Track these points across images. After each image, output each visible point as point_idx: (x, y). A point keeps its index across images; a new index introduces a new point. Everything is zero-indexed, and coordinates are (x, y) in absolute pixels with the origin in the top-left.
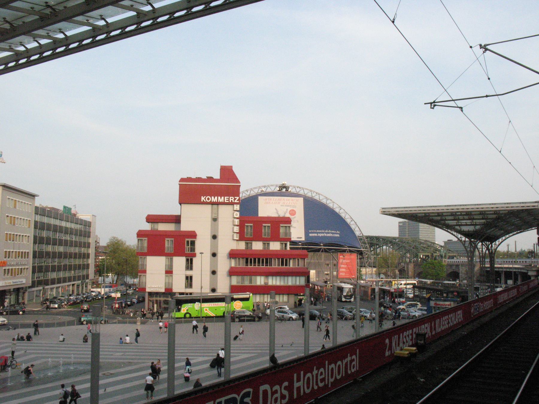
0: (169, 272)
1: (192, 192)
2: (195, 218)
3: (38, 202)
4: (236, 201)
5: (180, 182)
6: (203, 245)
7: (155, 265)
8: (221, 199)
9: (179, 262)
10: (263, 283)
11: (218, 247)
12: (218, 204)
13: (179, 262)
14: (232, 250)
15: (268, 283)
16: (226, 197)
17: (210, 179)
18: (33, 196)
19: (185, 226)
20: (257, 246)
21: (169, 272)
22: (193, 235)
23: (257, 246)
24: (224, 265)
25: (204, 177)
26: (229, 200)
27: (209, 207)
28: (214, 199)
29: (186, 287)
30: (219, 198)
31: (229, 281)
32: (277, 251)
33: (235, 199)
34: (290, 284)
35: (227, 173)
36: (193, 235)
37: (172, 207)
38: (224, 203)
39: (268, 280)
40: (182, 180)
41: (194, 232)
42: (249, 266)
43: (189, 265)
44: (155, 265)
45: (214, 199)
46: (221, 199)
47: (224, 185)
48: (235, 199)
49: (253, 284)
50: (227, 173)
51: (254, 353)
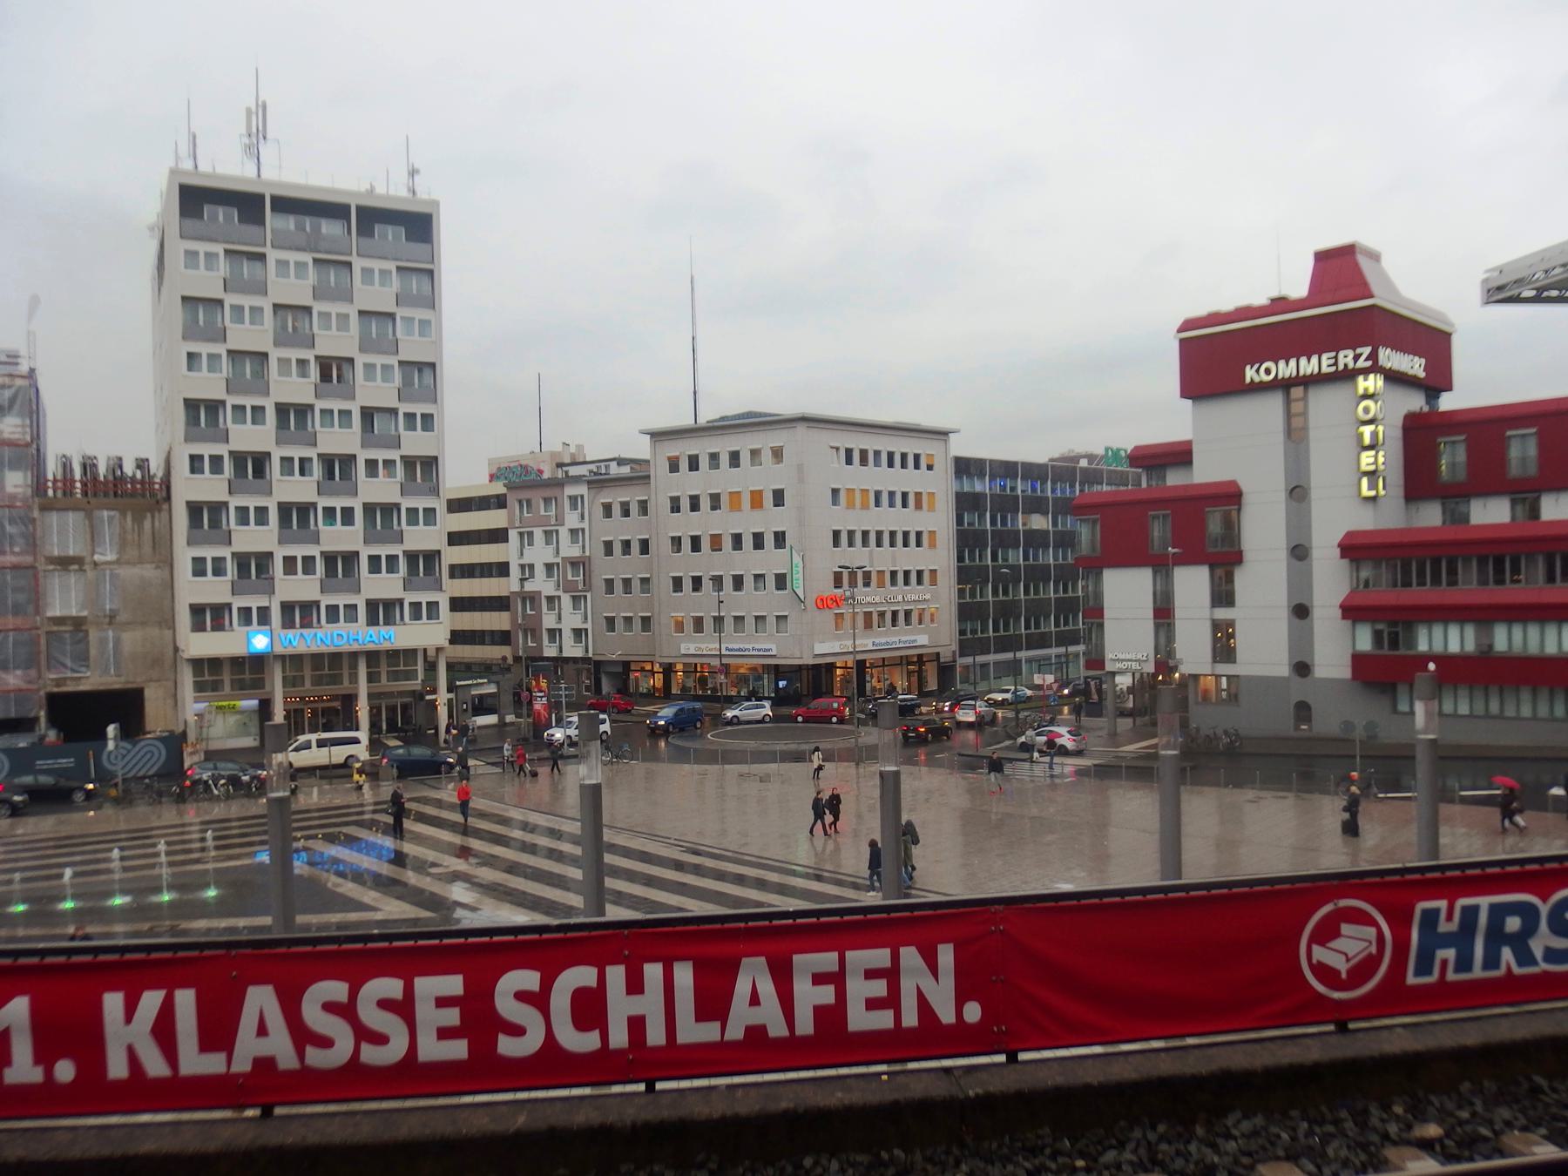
0: (1164, 613)
1: (1216, 359)
2: (1235, 444)
3: (960, 447)
4: (1361, 363)
5: (1180, 330)
6: (1262, 530)
7: (1126, 593)
8: (1308, 366)
9: (1192, 583)
10: (1470, 647)
11: (1309, 527)
12: (1308, 381)
13: (1192, 583)
14: (1349, 535)
15: (1491, 646)
16: (1325, 357)
17: (1280, 304)
18: (942, 434)
19: (1205, 471)
20: (1491, 513)
21: (1164, 613)
22: (1229, 496)
23: (1491, 513)
24: (1331, 582)
25: (1260, 299)
26: (1336, 364)
27: (1275, 402)
28: (1286, 369)
29: (1215, 661)
30: (1303, 361)
31: (1350, 643)
32: (1435, 529)
33: (1356, 358)
34: (1533, 649)
35: (1339, 267)
36: (1229, 496)
37: (1167, 416)
38: (1319, 379)
39: (1491, 636)
40: (1188, 325)
41: (1233, 483)
42: (1460, 586)
43: (1223, 595)
44: (1126, 593)
45: (1286, 369)
46: (1308, 366)
47: (1345, 314)
48: (1356, 358)
49: (1402, 652)
50: (1339, 267)
51: (534, 904)
